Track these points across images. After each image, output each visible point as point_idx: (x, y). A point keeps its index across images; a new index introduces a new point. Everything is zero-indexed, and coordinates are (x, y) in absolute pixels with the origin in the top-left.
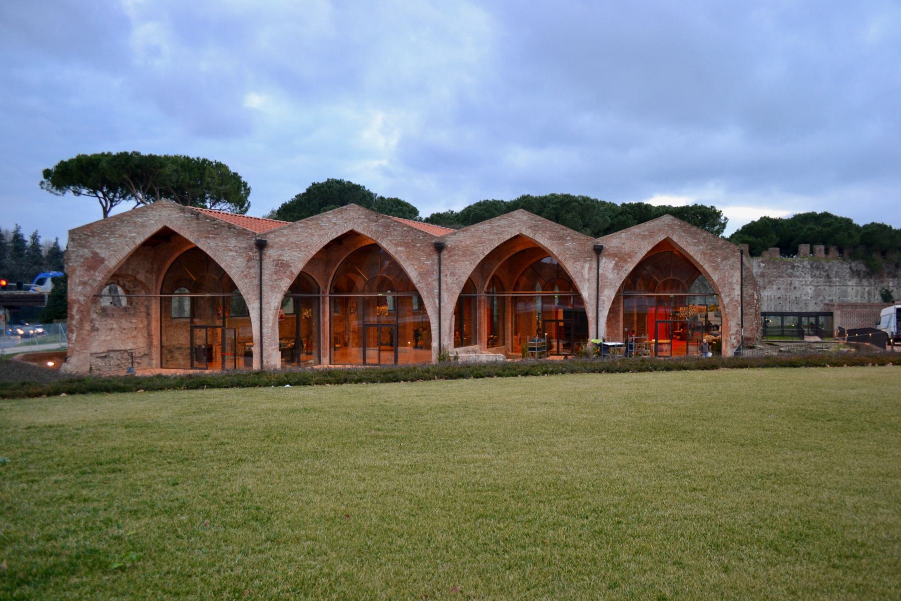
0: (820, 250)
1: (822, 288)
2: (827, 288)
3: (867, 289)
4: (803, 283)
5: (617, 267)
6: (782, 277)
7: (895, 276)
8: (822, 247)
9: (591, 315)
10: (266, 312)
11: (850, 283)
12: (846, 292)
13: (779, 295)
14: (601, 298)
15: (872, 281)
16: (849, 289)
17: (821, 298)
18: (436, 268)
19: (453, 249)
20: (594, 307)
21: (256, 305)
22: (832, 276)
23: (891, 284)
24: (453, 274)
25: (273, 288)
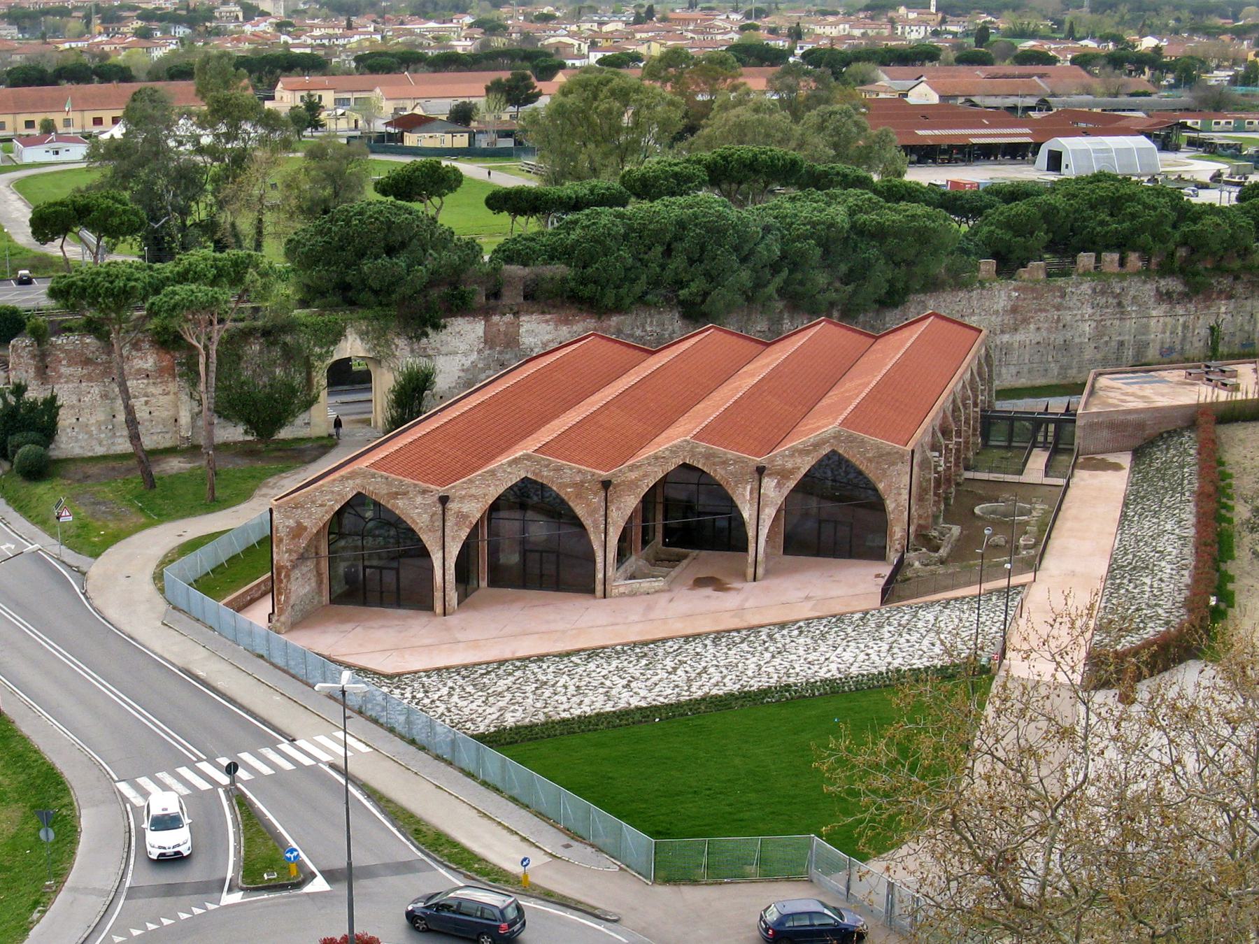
0: (1112, 261)
1: (1108, 323)
2: (1117, 322)
3: (1181, 320)
4: (1079, 317)
5: (779, 485)
6: (1045, 311)
7: (1230, 297)
8: (1116, 256)
9: (751, 534)
10: (443, 563)
11: (1154, 313)
12: (1146, 326)
13: (1039, 339)
14: (762, 517)
15: (1191, 307)
16: (1153, 322)
17: (1106, 338)
18: (603, 504)
19: (619, 485)
20: (755, 527)
21: (440, 554)
22: (1125, 303)
23: (1223, 309)
24: (618, 509)
25: (453, 538)
